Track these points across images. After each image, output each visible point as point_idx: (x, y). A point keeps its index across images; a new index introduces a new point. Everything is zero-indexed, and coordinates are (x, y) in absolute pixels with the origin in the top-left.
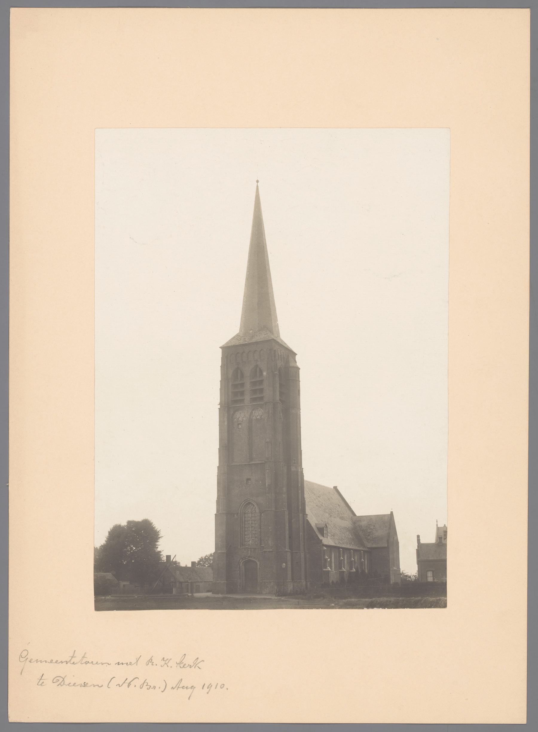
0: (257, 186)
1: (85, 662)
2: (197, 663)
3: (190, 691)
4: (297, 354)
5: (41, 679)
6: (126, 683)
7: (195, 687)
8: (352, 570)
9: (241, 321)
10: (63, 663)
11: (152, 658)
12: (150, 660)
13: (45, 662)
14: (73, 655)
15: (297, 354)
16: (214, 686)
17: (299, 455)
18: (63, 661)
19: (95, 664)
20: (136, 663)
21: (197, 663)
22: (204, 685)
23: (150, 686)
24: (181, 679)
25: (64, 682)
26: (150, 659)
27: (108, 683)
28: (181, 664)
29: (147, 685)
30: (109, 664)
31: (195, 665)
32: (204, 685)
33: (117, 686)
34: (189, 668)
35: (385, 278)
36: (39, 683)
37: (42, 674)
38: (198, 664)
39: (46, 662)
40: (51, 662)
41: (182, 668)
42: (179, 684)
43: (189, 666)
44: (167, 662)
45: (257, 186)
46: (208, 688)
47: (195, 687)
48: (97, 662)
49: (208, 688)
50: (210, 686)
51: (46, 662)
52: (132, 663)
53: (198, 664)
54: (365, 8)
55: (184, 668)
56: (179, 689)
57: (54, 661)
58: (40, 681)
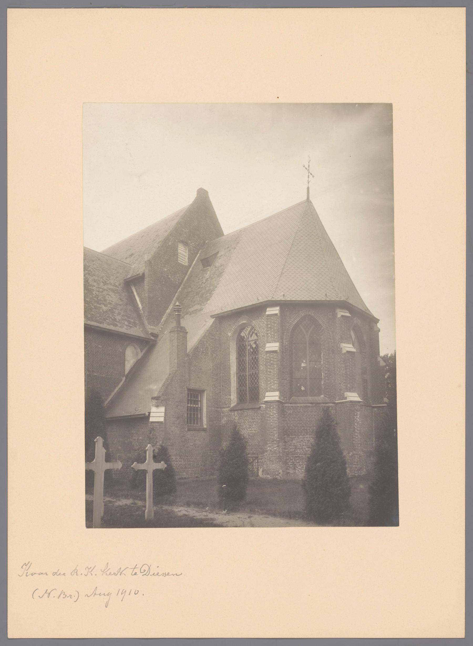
0: (308, 188)
1: (39, 573)
3: (107, 597)
4: (380, 320)
6: (48, 593)
7: (111, 593)
11: (76, 568)
13: (177, 575)
14: (149, 567)
15: (380, 320)
16: (133, 592)
18: (172, 575)
22: (119, 590)
23: (66, 595)
26: (75, 568)
27: (33, 593)
29: (64, 595)
32: (119, 590)
33: (182, 573)
35: (292, 245)
36: (124, 595)
38: (123, 571)
41: (165, 576)
42: (95, 591)
44: (90, 570)
45: (308, 188)
46: (122, 594)
47: (111, 593)
49: (122, 594)
50: (123, 592)
54: (123, 7)
55: (154, 575)
56: (95, 596)
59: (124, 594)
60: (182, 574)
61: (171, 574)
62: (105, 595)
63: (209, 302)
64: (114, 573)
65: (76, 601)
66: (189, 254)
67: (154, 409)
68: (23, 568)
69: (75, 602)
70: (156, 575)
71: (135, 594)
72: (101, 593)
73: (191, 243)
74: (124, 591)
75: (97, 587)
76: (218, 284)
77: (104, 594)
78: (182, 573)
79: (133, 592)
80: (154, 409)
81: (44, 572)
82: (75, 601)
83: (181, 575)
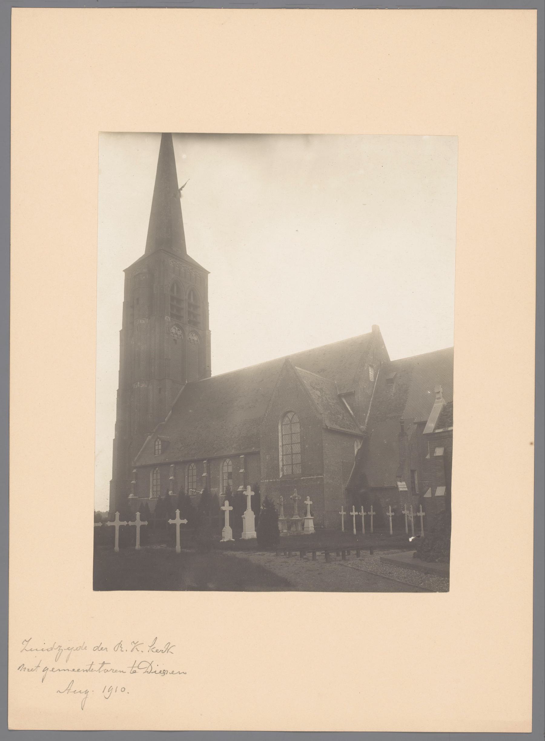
2: (168, 648)
5: (133, 667)
8: (241, 537)
9: (411, 358)
10: (35, 649)
12: (134, 673)
16: (119, 690)
17: (342, 431)
18: (60, 670)
19: (159, 673)
20: (192, 467)
21: (168, 648)
24: (84, 709)
25: (111, 692)
28: (152, 648)
30: (185, 673)
31: (167, 650)
34: (98, 673)
37: (117, 692)
38: (169, 649)
39: (68, 670)
40: (172, 673)
43: (112, 670)
46: (109, 692)
48: (32, 649)
49: (109, 692)
51: (68, 671)
52: (158, 650)
53: (169, 649)
57: (76, 670)
58: (133, 666)
59: (111, 692)
60: (138, 652)
61: (61, 671)
62: (81, 692)
63: (404, 411)
64: (59, 646)
65: (174, 646)
66: (374, 374)
67: (399, 483)
68: (23, 643)
69: (175, 646)
70: (84, 649)
71: (122, 691)
72: (75, 691)
73: (374, 365)
74: (87, 691)
75: (156, 638)
76: (407, 399)
77: (81, 691)
78: (138, 651)
79: (119, 690)
80: (399, 483)
81: (34, 648)
82: (174, 646)
83: (137, 651)
